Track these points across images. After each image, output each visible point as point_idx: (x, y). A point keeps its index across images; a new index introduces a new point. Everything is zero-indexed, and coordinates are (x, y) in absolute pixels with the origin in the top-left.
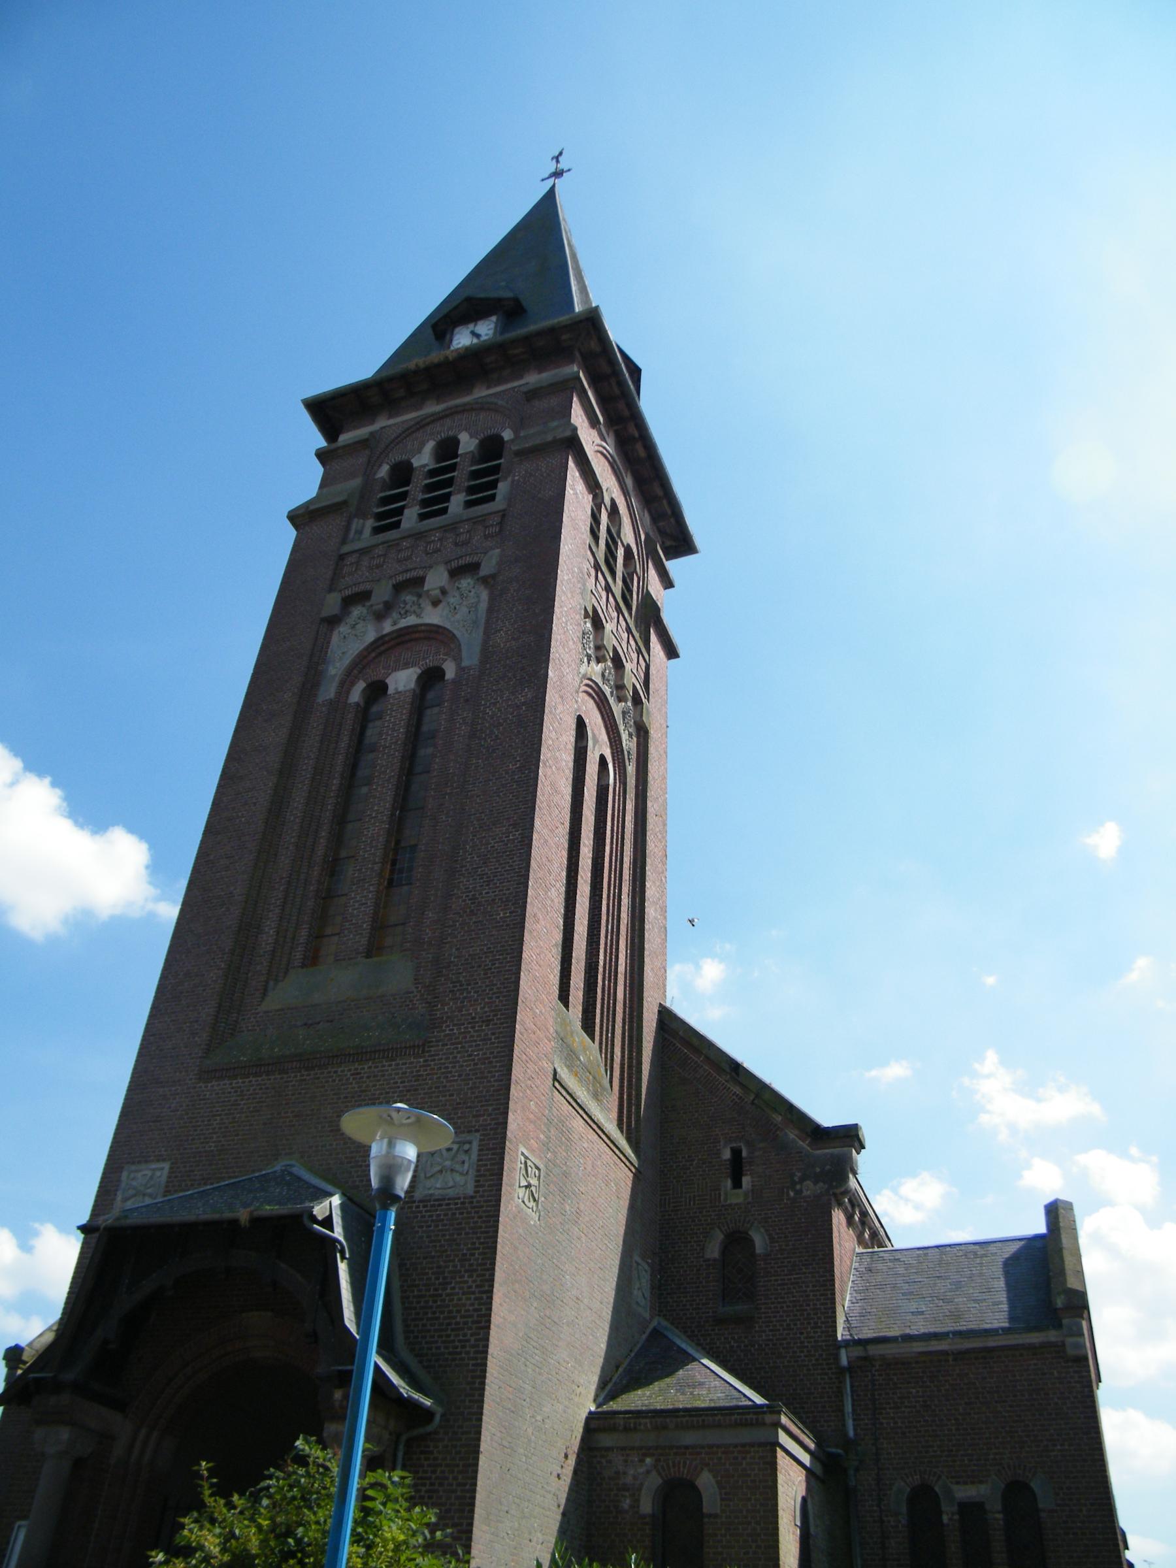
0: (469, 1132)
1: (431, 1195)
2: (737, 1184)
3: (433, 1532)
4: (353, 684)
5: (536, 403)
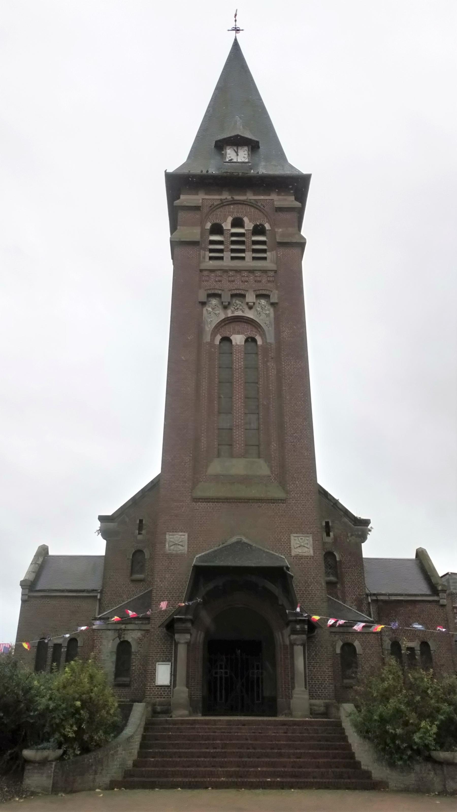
0: (308, 533)
1: (298, 555)
2: (328, 535)
3: (16, 675)
4: (215, 336)
5: (280, 214)
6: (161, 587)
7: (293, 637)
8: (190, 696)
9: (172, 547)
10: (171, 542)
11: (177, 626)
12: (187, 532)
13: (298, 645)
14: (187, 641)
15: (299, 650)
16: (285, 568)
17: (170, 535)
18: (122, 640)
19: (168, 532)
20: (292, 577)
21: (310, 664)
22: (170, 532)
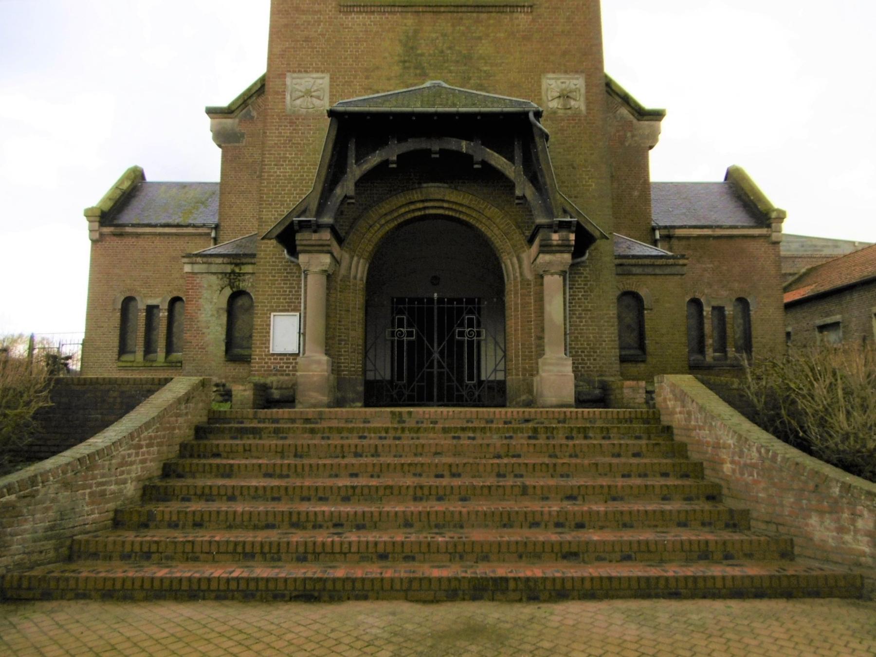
6: (278, 176)
7: (545, 258)
8: (336, 368)
9: (298, 102)
10: (297, 90)
11: (301, 238)
12: (328, 71)
13: (552, 274)
14: (324, 268)
15: (553, 283)
16: (531, 116)
17: (294, 78)
18: (234, 290)
19: (289, 71)
20: (546, 137)
21: (574, 314)
22: (294, 72)
